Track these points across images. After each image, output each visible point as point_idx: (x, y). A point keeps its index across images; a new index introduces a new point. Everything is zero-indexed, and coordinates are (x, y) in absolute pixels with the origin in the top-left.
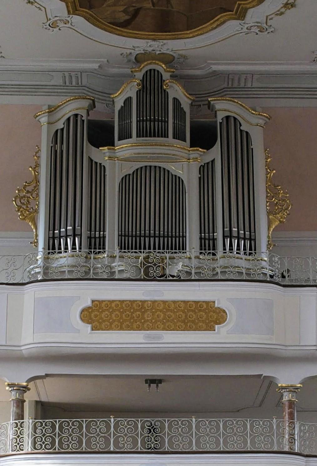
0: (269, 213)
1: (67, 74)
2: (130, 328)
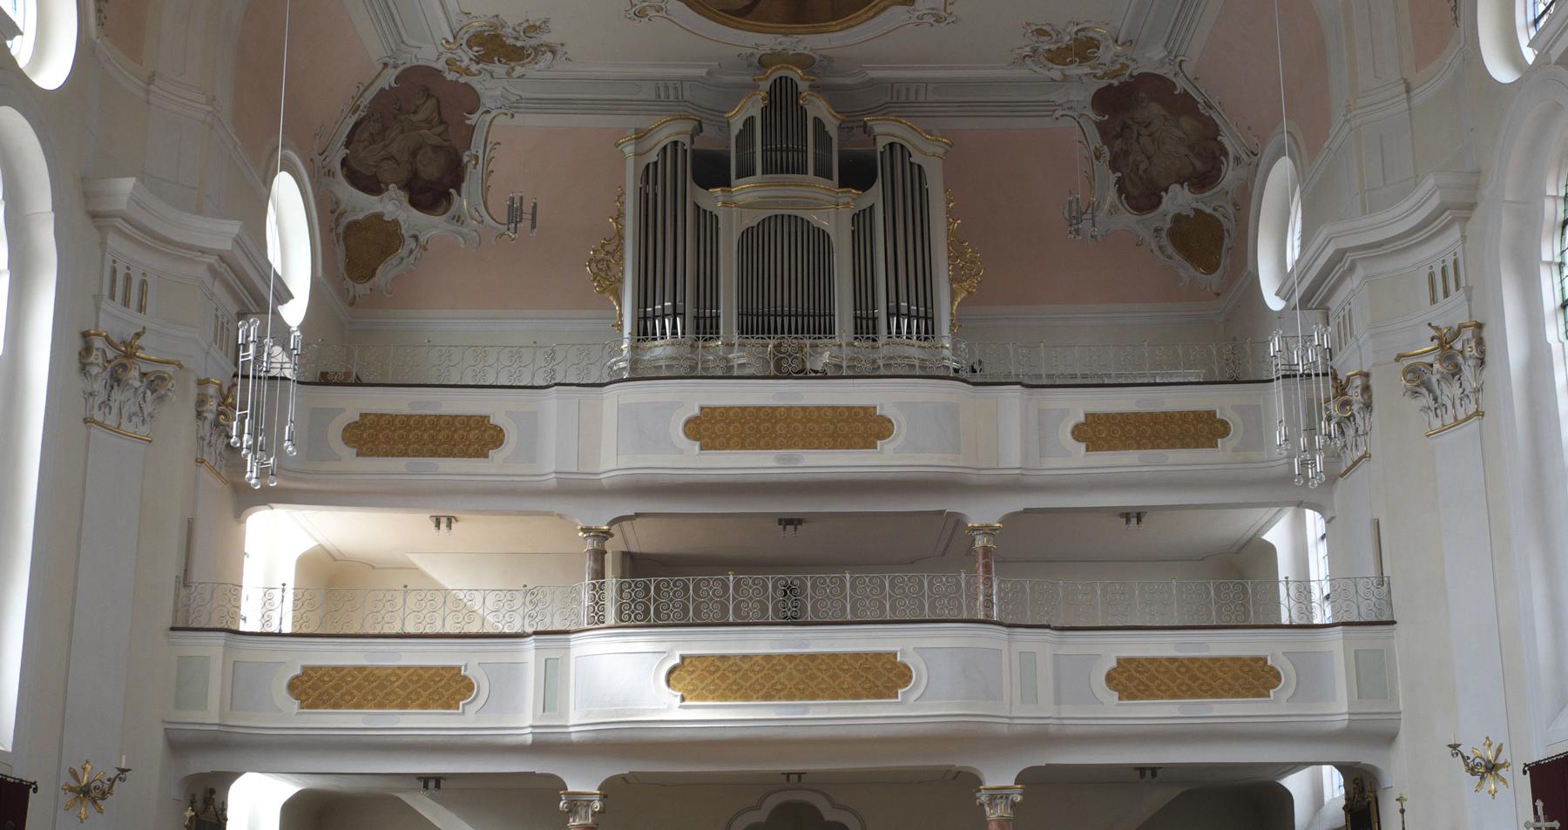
0: (952, 280)
1: (661, 84)
2: (756, 446)
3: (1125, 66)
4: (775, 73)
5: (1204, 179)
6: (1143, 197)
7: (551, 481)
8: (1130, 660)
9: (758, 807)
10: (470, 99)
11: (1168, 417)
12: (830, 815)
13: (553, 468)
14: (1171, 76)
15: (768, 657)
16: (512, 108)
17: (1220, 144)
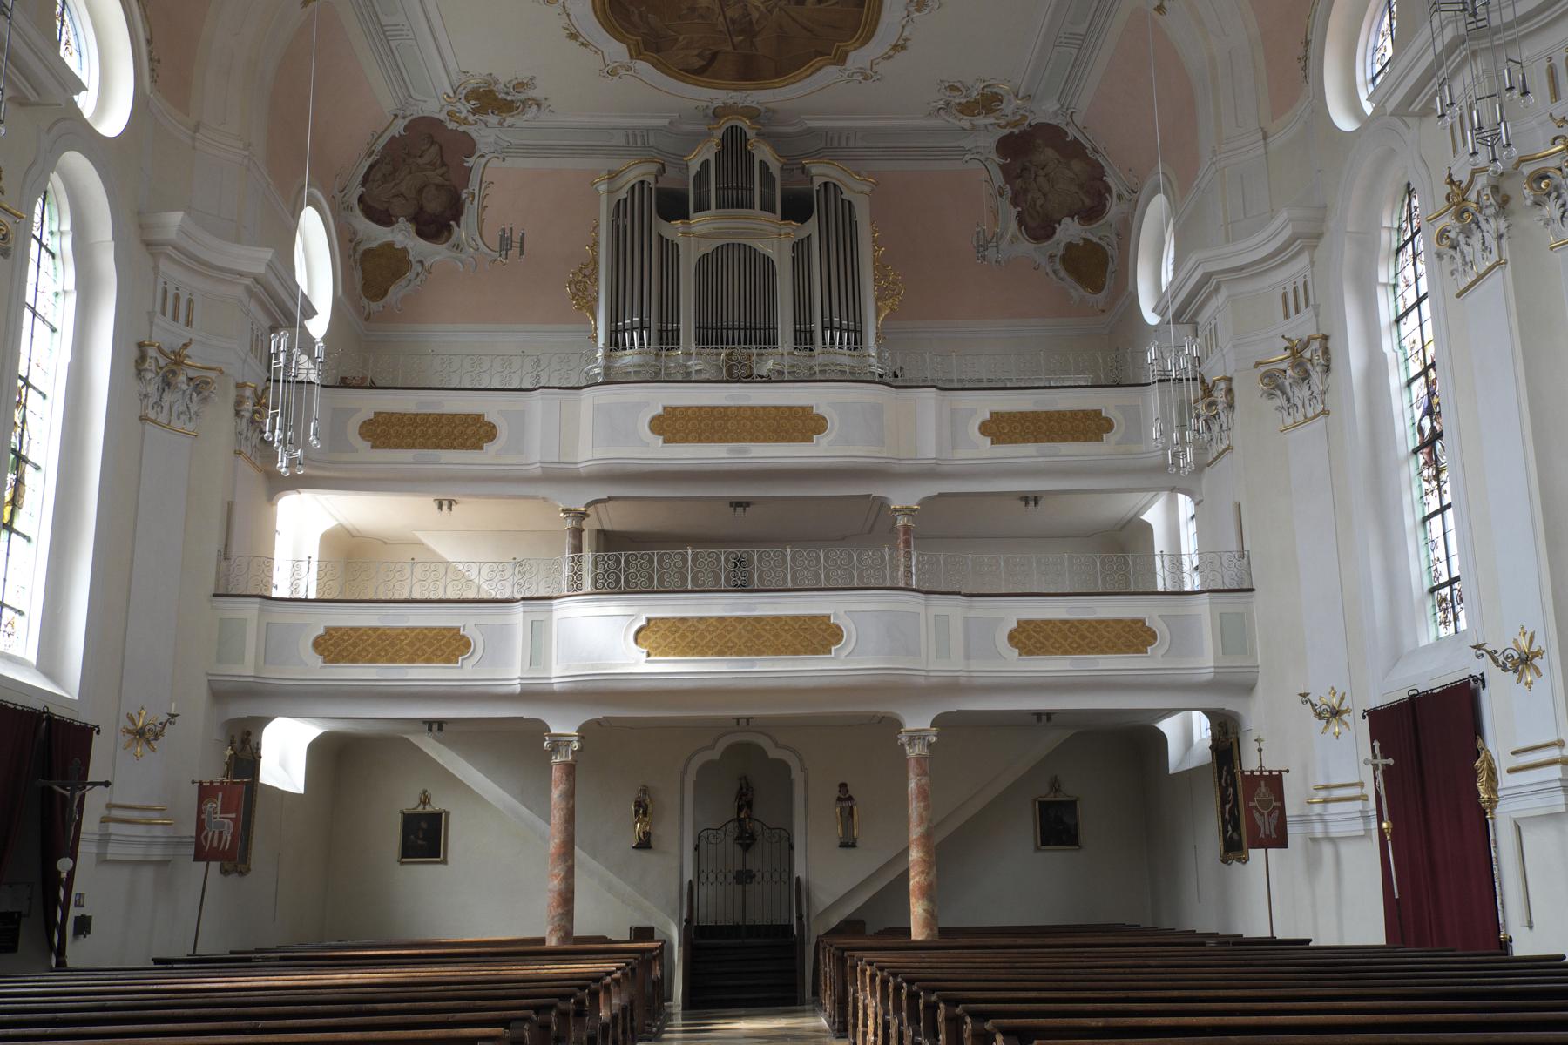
0: (877, 299)
2: (710, 440)
3: (1024, 117)
4: (726, 123)
5: (1092, 213)
6: (1039, 227)
7: (537, 470)
8: (1028, 622)
9: (712, 747)
10: (470, 146)
11: (1061, 415)
12: (774, 753)
13: (538, 458)
14: (1063, 126)
15: (721, 619)
16: (504, 153)
17: (1105, 182)
